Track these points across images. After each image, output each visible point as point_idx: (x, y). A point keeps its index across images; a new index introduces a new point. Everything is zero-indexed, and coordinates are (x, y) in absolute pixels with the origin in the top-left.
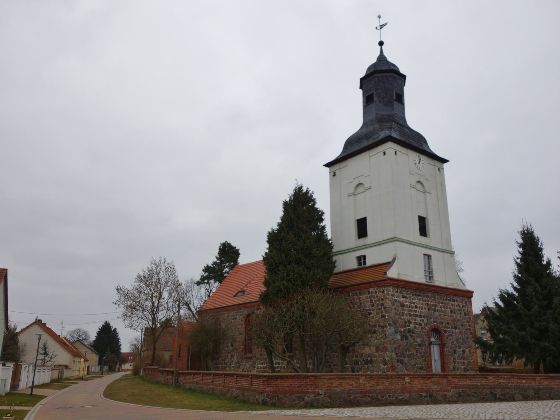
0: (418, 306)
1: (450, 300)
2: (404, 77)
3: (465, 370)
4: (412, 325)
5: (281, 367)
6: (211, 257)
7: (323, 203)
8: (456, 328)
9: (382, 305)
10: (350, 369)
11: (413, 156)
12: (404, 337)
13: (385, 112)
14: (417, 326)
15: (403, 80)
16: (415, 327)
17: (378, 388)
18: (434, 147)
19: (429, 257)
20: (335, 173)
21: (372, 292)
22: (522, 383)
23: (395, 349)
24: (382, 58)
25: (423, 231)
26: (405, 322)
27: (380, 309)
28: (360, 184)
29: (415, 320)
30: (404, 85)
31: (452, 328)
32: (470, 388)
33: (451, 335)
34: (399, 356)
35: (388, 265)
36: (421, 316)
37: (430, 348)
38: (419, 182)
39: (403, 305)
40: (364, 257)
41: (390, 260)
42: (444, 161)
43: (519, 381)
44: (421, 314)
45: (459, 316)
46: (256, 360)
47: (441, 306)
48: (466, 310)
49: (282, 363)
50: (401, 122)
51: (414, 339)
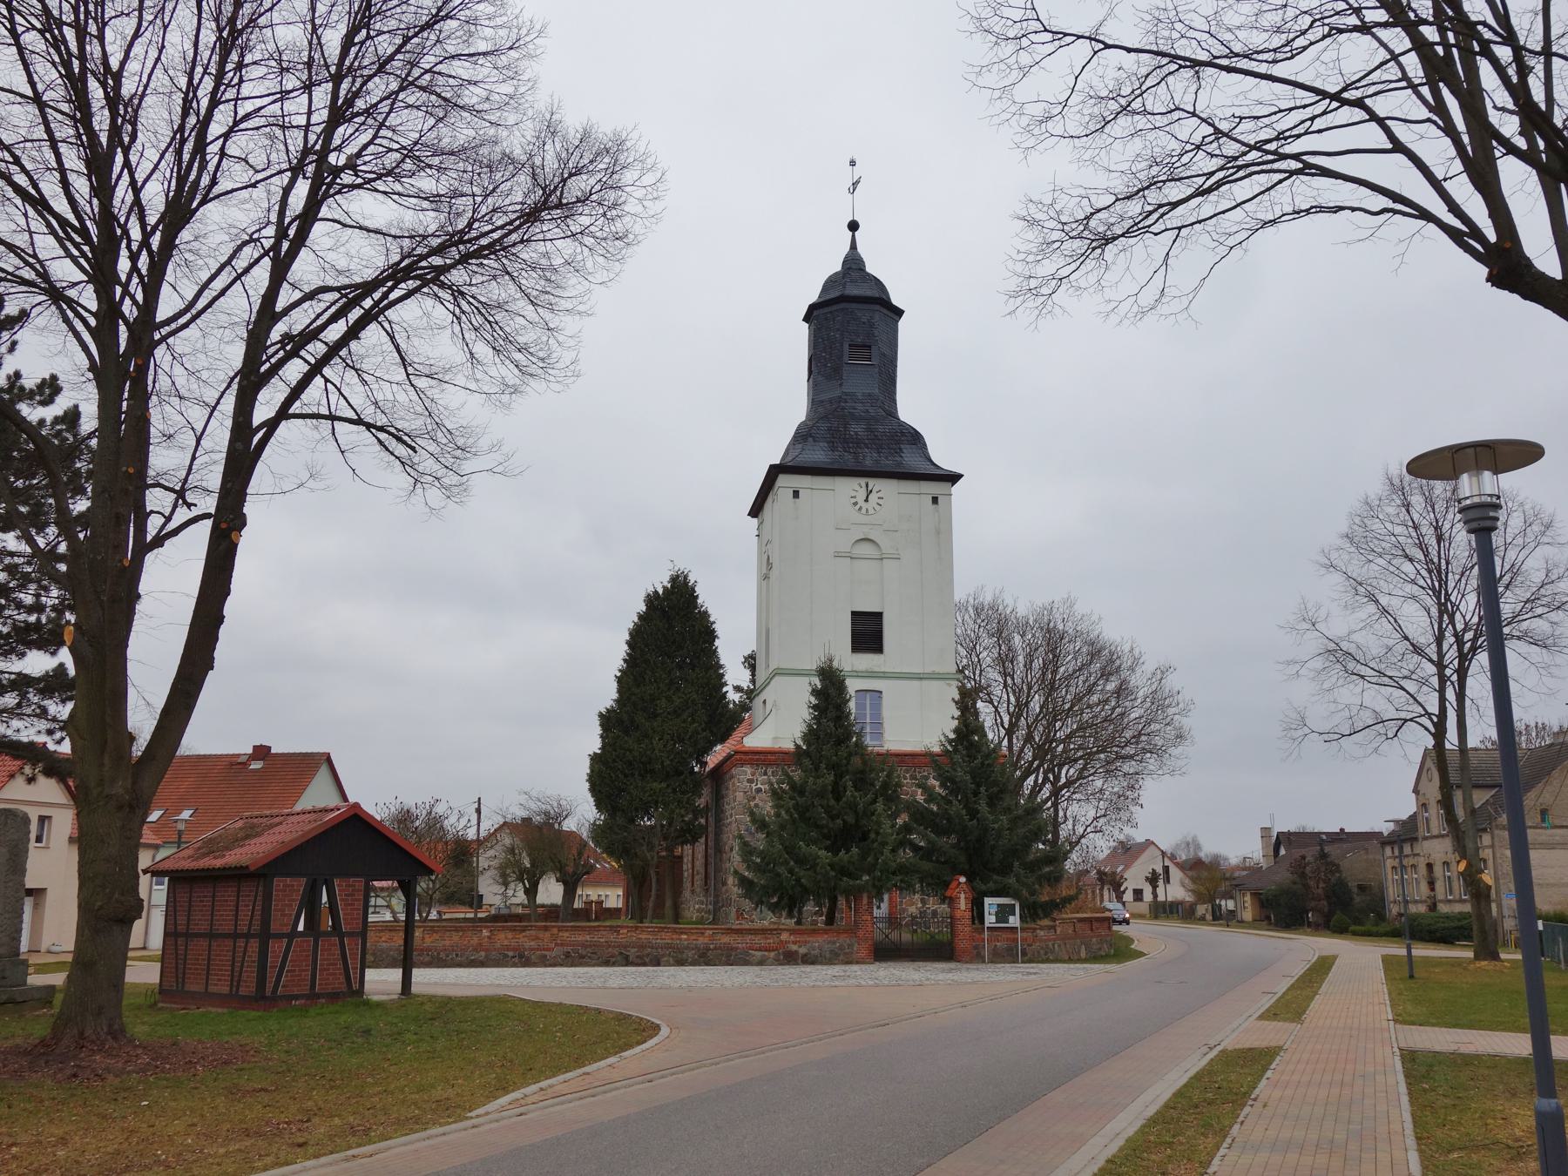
2: (899, 313)
17: (440, 944)
24: (853, 263)
32: (584, 946)
42: (954, 478)
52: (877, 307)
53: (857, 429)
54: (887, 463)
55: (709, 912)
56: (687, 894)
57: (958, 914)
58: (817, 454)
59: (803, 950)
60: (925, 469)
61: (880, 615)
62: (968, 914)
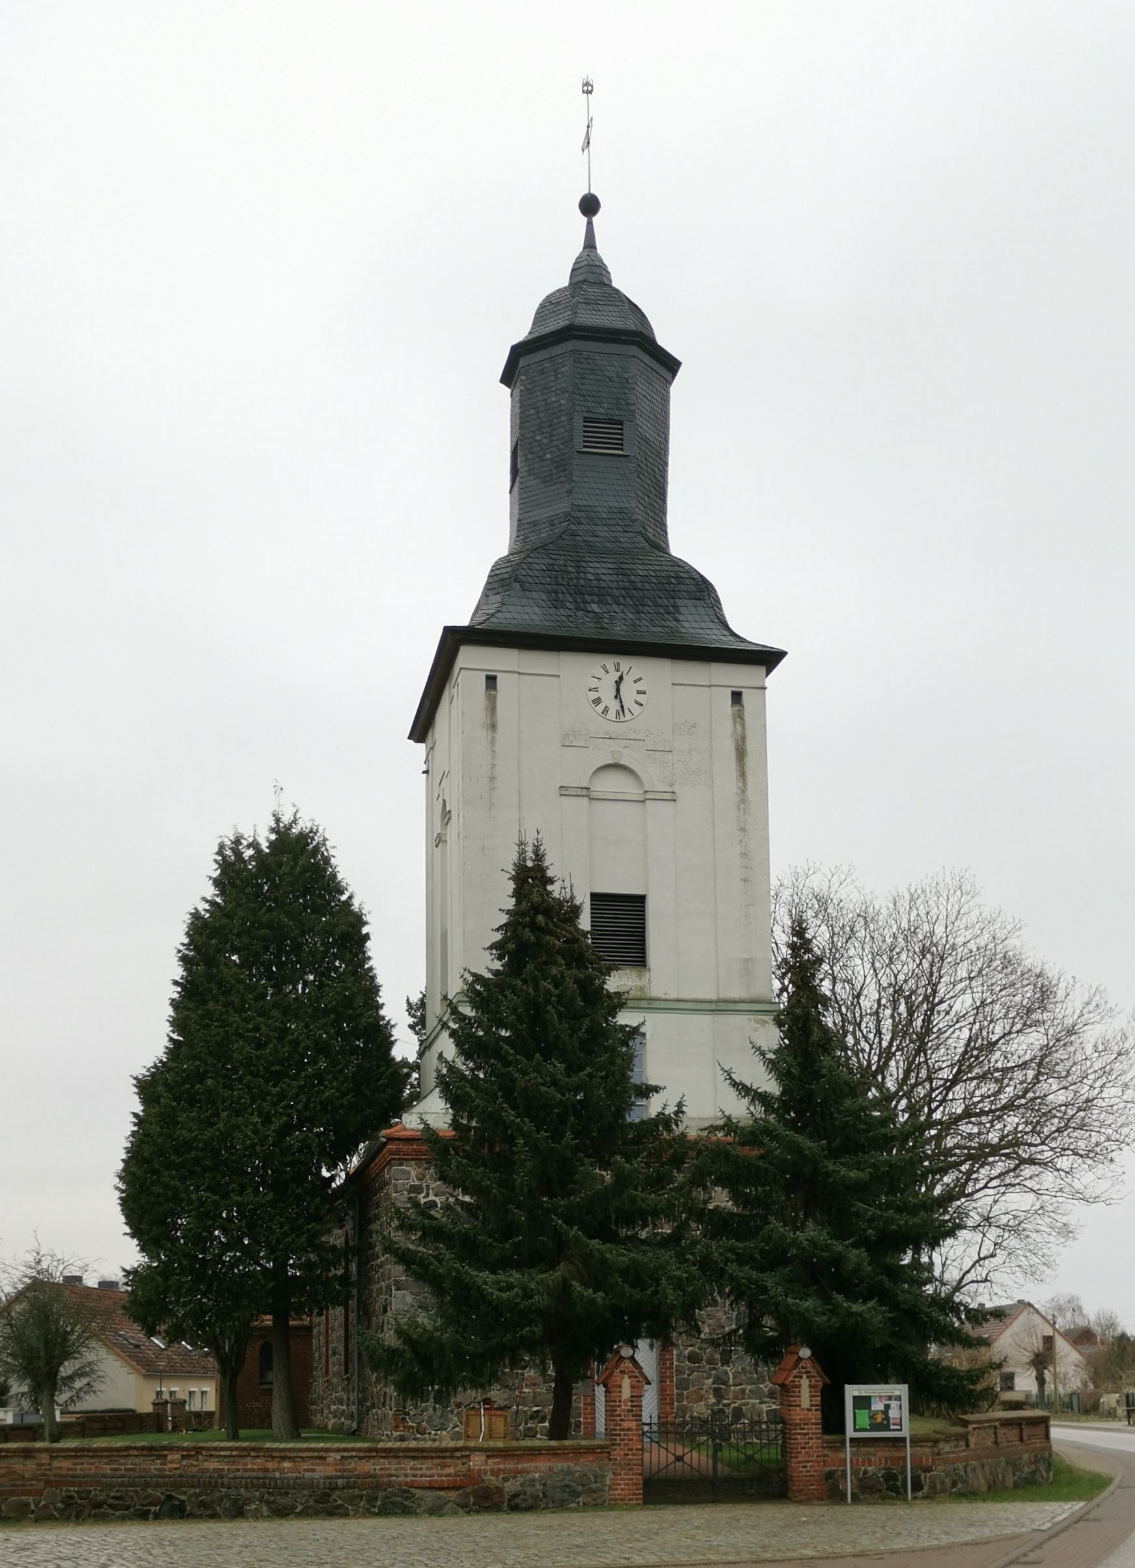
2: (671, 365)
22: (281, 1470)
24: (590, 273)
42: (769, 658)
43: (270, 1465)
52: (634, 350)
53: (600, 570)
54: (653, 632)
55: (351, 1417)
56: (319, 1386)
57: (797, 1415)
58: (528, 614)
59: (511, 1486)
60: (714, 638)
61: (640, 900)
62: (816, 1416)
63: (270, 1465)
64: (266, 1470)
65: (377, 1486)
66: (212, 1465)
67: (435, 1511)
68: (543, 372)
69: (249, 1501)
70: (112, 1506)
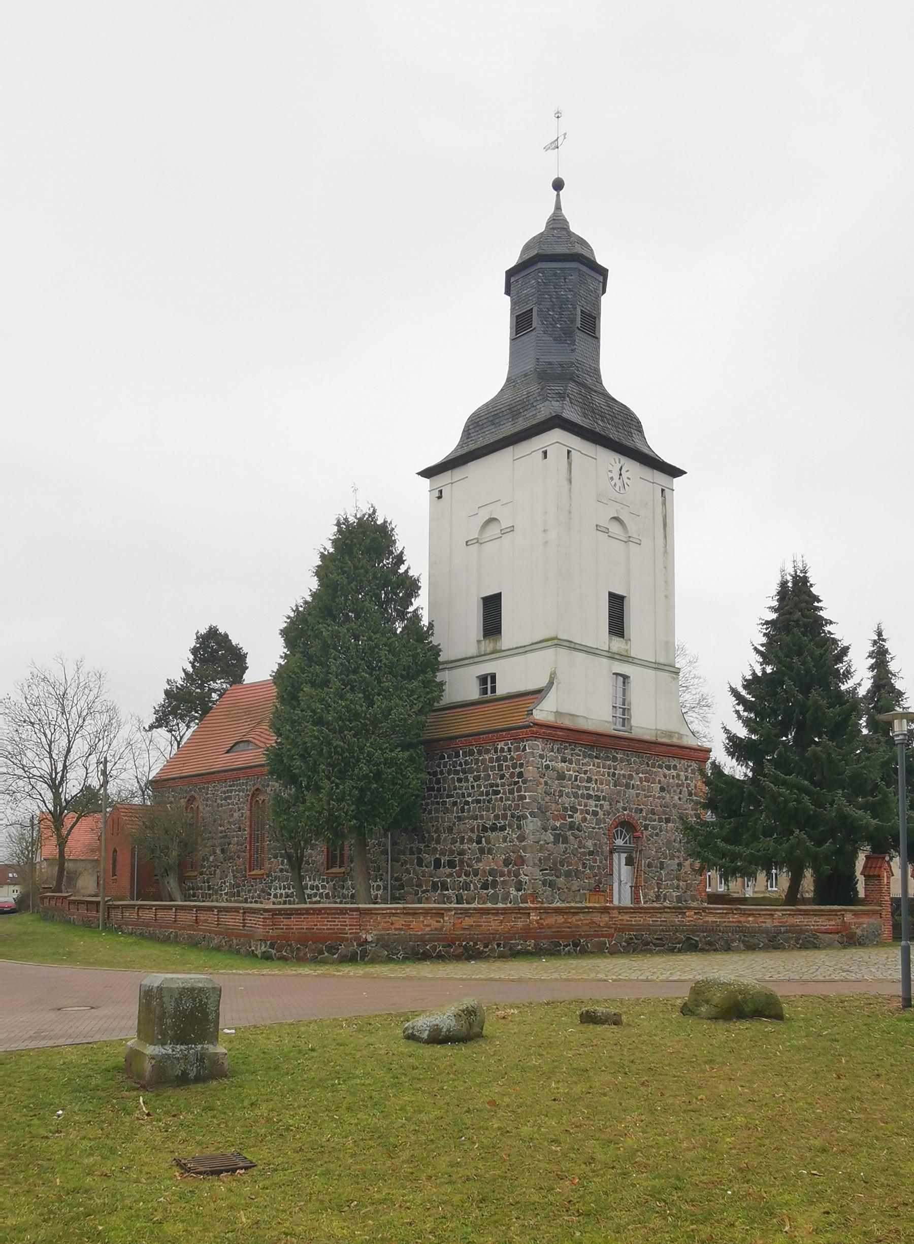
0: (594, 778)
1: (660, 767)
3: (679, 899)
4: (578, 816)
5: (321, 895)
6: (177, 664)
7: (416, 555)
8: (668, 821)
9: (520, 775)
10: (454, 899)
11: (609, 460)
12: (560, 838)
13: (557, 356)
14: (588, 817)
15: (601, 278)
16: (584, 820)
18: (658, 442)
19: (625, 678)
20: (441, 492)
21: (502, 750)
23: (540, 860)
24: (558, 223)
25: (617, 626)
26: (565, 809)
27: (516, 783)
28: (492, 520)
29: (586, 806)
30: (604, 292)
31: (660, 820)
33: (657, 835)
34: (547, 875)
35: (539, 694)
36: (598, 798)
37: (612, 859)
38: (616, 519)
39: (561, 777)
40: (493, 677)
41: (542, 683)
43: (742, 919)
44: (599, 793)
45: (676, 798)
46: (272, 881)
47: (641, 778)
48: (692, 785)
49: (324, 887)
50: (589, 381)
51: (580, 842)
63: (742, 919)
64: (740, 922)
65: (802, 932)
66: (710, 919)
67: (829, 946)
68: (555, 275)
69: (733, 941)
70: (654, 944)
